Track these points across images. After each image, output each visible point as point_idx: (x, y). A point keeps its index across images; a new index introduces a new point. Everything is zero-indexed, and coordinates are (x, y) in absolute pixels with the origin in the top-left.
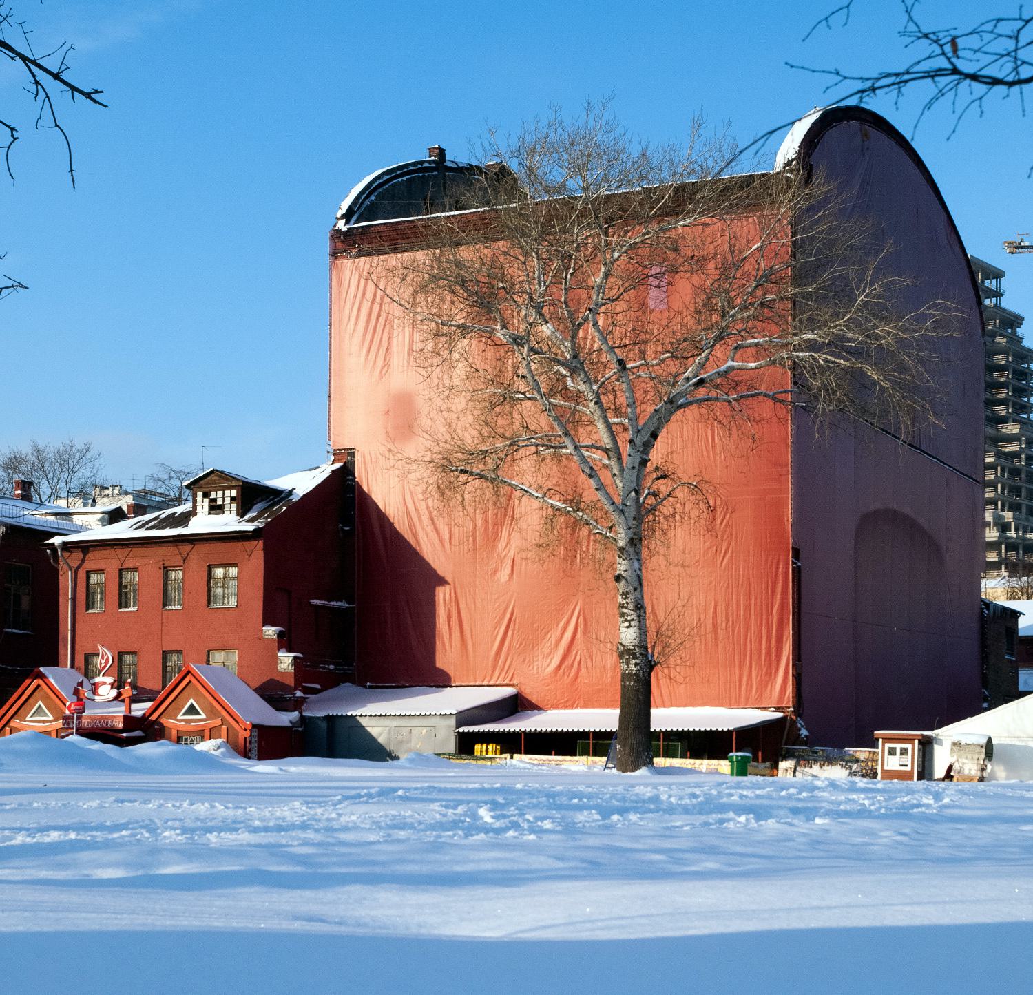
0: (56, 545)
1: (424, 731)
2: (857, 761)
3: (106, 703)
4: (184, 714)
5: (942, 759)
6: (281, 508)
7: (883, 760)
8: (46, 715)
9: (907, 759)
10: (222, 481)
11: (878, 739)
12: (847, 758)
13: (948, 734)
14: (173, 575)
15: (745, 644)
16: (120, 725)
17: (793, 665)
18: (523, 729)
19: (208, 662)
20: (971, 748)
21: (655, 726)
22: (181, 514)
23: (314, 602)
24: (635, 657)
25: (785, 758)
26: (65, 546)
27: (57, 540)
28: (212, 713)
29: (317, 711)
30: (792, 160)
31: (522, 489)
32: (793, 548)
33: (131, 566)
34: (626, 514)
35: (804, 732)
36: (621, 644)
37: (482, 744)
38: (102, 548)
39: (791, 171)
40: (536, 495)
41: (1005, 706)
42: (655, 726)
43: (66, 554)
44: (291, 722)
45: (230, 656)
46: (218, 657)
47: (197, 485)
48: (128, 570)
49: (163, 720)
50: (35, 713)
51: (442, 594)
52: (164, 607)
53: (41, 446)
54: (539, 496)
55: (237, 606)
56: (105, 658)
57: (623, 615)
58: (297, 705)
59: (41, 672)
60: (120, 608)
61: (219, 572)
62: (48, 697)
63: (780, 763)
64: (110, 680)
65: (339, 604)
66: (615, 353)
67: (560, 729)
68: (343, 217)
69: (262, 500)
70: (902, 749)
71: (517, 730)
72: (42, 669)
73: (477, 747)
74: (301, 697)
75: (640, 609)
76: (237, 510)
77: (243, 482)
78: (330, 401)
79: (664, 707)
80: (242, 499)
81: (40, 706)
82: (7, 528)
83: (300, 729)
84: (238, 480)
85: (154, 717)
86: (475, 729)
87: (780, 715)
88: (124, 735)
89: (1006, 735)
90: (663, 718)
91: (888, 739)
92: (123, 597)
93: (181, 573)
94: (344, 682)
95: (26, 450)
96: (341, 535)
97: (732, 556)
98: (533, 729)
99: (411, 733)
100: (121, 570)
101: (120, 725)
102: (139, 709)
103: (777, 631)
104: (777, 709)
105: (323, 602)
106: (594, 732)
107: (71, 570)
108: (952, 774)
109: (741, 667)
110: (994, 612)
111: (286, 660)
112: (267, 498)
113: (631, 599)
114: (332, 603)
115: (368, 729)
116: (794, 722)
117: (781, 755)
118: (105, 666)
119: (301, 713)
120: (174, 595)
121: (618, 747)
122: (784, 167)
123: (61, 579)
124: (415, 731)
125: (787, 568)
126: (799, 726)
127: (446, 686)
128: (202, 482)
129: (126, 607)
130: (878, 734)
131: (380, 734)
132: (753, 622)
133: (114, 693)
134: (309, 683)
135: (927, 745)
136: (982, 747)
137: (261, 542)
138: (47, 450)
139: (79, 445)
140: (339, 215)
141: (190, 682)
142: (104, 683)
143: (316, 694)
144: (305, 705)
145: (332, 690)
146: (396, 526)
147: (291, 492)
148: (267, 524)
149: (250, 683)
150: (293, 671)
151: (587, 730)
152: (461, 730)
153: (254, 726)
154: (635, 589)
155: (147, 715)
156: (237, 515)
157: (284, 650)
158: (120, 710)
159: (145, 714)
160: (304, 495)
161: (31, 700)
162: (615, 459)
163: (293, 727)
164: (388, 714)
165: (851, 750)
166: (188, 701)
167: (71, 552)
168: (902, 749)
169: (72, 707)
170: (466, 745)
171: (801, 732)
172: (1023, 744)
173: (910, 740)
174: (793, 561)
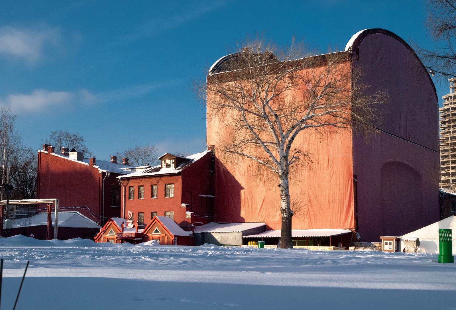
0: (119, 178)
1: (232, 238)
2: (375, 247)
3: (130, 229)
4: (154, 232)
5: (403, 245)
6: (188, 165)
7: (383, 246)
9: (391, 246)
10: (170, 157)
11: (381, 239)
12: (372, 246)
13: (405, 237)
14: (154, 187)
15: (339, 208)
16: (134, 236)
17: (354, 214)
18: (263, 237)
19: (165, 215)
20: (411, 242)
21: (293, 235)
23: (200, 195)
24: (286, 212)
25: (351, 246)
26: (122, 179)
27: (120, 177)
28: (163, 232)
29: (199, 231)
30: (351, 47)
31: (250, 157)
32: (353, 175)
33: (142, 185)
34: (281, 165)
35: (359, 237)
36: (281, 207)
37: (251, 241)
38: (134, 179)
39: (351, 51)
40: (255, 159)
41: (424, 227)
42: (293, 235)
43: (122, 182)
44: (189, 235)
45: (172, 213)
46: (168, 214)
47: (163, 158)
48: (141, 186)
49: (148, 234)
51: (242, 192)
52: (152, 198)
54: (256, 159)
55: (174, 197)
57: (282, 198)
58: (192, 229)
60: (139, 198)
61: (168, 186)
62: (114, 227)
63: (350, 247)
64: (131, 221)
65: (210, 196)
66: (274, 113)
67: (274, 236)
68: (211, 71)
69: (184, 163)
70: (389, 243)
71: (261, 237)
72: (112, 218)
73: (249, 243)
74: (193, 227)
75: (287, 196)
77: (176, 157)
79: (313, 229)
80: (176, 163)
81: (112, 230)
82: (110, 173)
85: (145, 233)
86: (248, 236)
87: (350, 231)
88: (135, 239)
89: (432, 238)
90: (296, 233)
91: (384, 239)
92: (140, 195)
96: (210, 173)
97: (334, 178)
98: (266, 237)
99: (228, 238)
101: (134, 236)
102: (141, 231)
103: (103, 198)
104: (350, 229)
106: (308, 237)
108: (405, 251)
109: (337, 215)
110: (445, 196)
111: (189, 214)
112: (185, 162)
113: (284, 192)
114: (207, 196)
116: (355, 234)
117: (350, 245)
118: (130, 217)
119: (193, 232)
120: (155, 194)
121: (281, 242)
122: (348, 50)
125: (352, 182)
126: (357, 235)
127: (243, 223)
128: (164, 158)
130: (381, 238)
131: (218, 239)
132: (341, 200)
133: (132, 226)
135: (398, 241)
136: (415, 242)
137: (181, 176)
140: (210, 71)
141: (156, 222)
142: (129, 223)
144: (195, 229)
145: (207, 224)
147: (193, 160)
148: (183, 170)
149: (178, 222)
151: (305, 236)
152: (243, 237)
153: (175, 236)
154: (285, 189)
156: (175, 168)
157: (188, 211)
158: (134, 231)
159: (142, 232)
161: (109, 228)
162: (279, 147)
163: (190, 236)
164: (216, 232)
165: (373, 243)
168: (389, 243)
170: (245, 242)
171: (358, 237)
172: (431, 241)
173: (392, 239)
174: (354, 179)
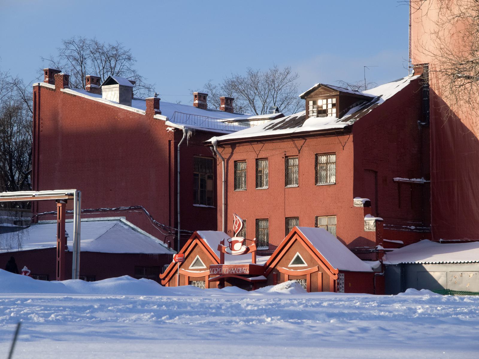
0: (212, 143)
1: (471, 275)
3: (240, 257)
6: (368, 110)
8: (202, 265)
10: (326, 92)
14: (291, 162)
16: (247, 272)
19: (316, 225)
22: (301, 117)
23: (397, 179)
26: (219, 144)
28: (312, 263)
29: (395, 259)
33: (264, 156)
43: (220, 150)
44: (373, 269)
45: (332, 220)
46: (324, 221)
49: (278, 268)
50: (194, 264)
52: (286, 186)
53: (255, 71)
55: (335, 184)
56: (238, 223)
58: (379, 256)
59: (197, 234)
60: (257, 187)
61: (323, 159)
62: (203, 252)
64: (241, 239)
65: (419, 180)
69: (357, 105)
72: (198, 232)
74: (381, 250)
76: (337, 113)
78: (410, 29)
81: (198, 259)
83: (381, 274)
84: (337, 91)
85: (272, 266)
88: (250, 279)
92: (259, 179)
93: (297, 160)
94: (423, 239)
95: (244, 75)
96: (419, 128)
99: (461, 276)
100: (257, 160)
101: (247, 272)
102: (262, 261)
105: (405, 179)
107: (224, 161)
111: (370, 222)
114: (412, 180)
115: (430, 273)
119: (381, 262)
120: (294, 176)
123: (218, 167)
124: (465, 275)
128: (312, 94)
129: (261, 186)
131: (440, 277)
133: (244, 249)
134: (394, 239)
137: (351, 136)
138: (259, 74)
139: (281, 70)
141: (296, 240)
143: (399, 248)
146: (462, 121)
147: (379, 98)
150: (375, 230)
153: (340, 272)
155: (267, 265)
156: (337, 117)
157: (369, 215)
158: (248, 261)
159: (266, 263)
160: (387, 100)
161: (192, 254)
163: (374, 273)
166: (296, 253)
167: (224, 148)
169: (177, 258)
